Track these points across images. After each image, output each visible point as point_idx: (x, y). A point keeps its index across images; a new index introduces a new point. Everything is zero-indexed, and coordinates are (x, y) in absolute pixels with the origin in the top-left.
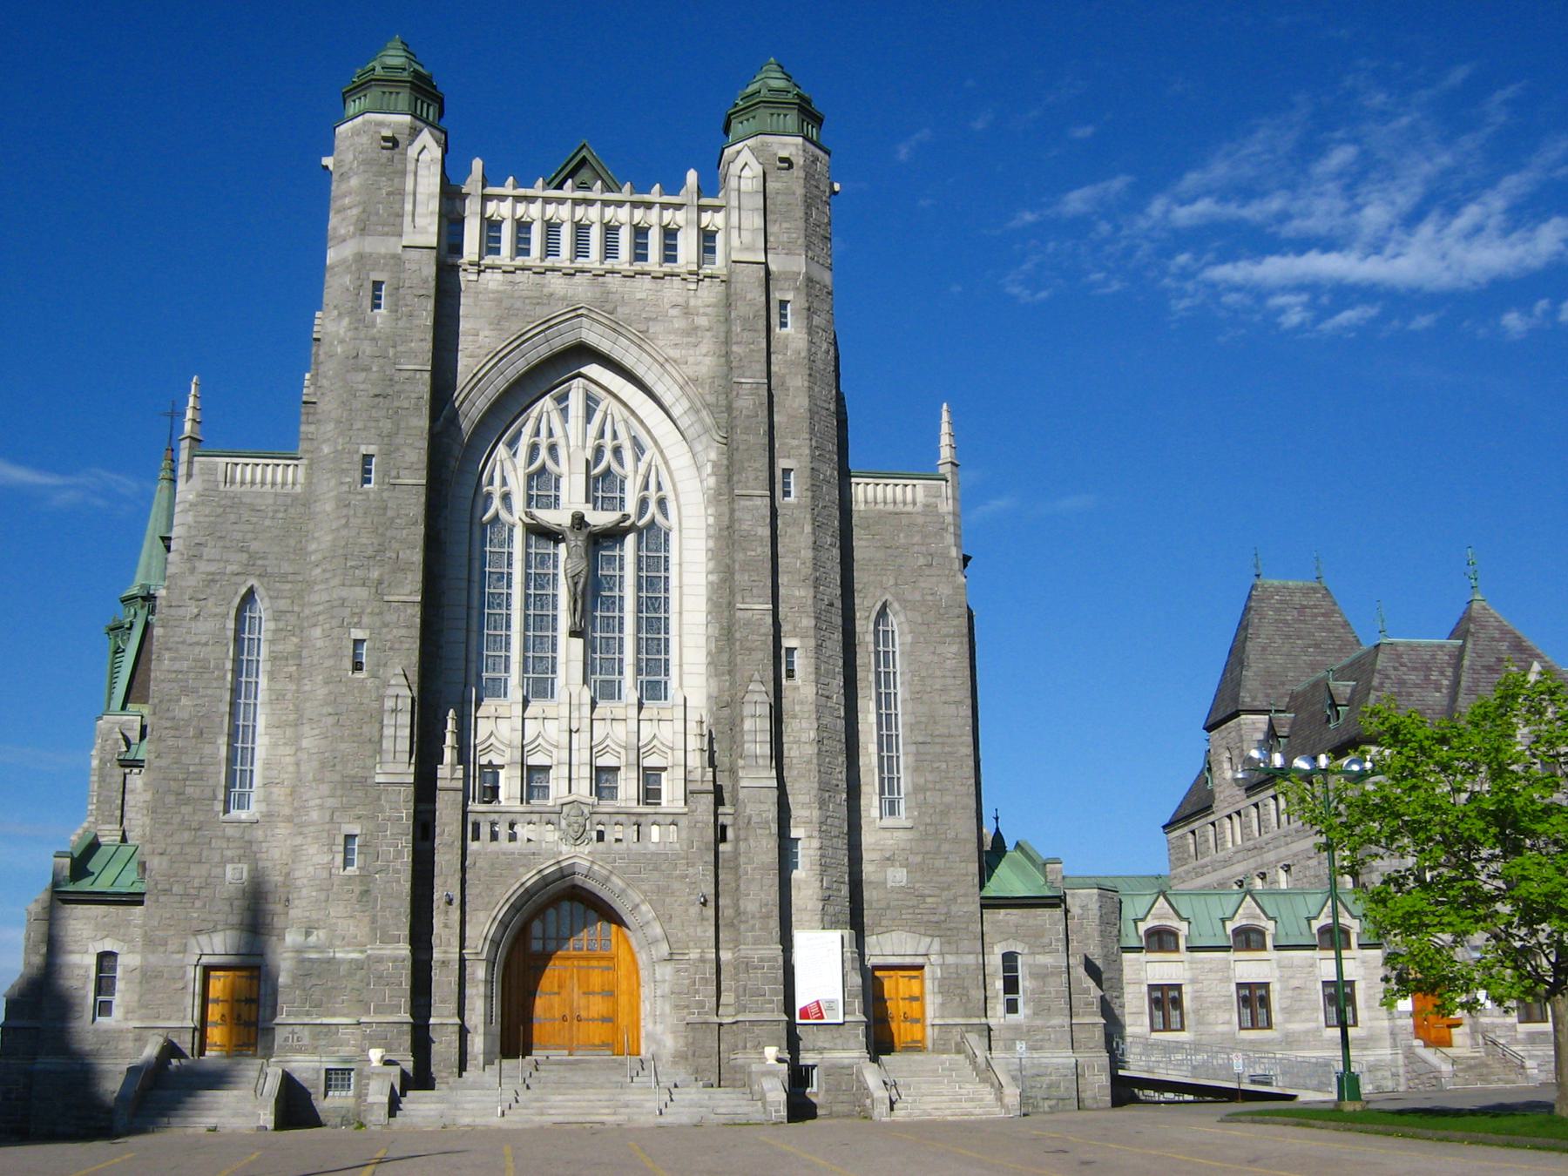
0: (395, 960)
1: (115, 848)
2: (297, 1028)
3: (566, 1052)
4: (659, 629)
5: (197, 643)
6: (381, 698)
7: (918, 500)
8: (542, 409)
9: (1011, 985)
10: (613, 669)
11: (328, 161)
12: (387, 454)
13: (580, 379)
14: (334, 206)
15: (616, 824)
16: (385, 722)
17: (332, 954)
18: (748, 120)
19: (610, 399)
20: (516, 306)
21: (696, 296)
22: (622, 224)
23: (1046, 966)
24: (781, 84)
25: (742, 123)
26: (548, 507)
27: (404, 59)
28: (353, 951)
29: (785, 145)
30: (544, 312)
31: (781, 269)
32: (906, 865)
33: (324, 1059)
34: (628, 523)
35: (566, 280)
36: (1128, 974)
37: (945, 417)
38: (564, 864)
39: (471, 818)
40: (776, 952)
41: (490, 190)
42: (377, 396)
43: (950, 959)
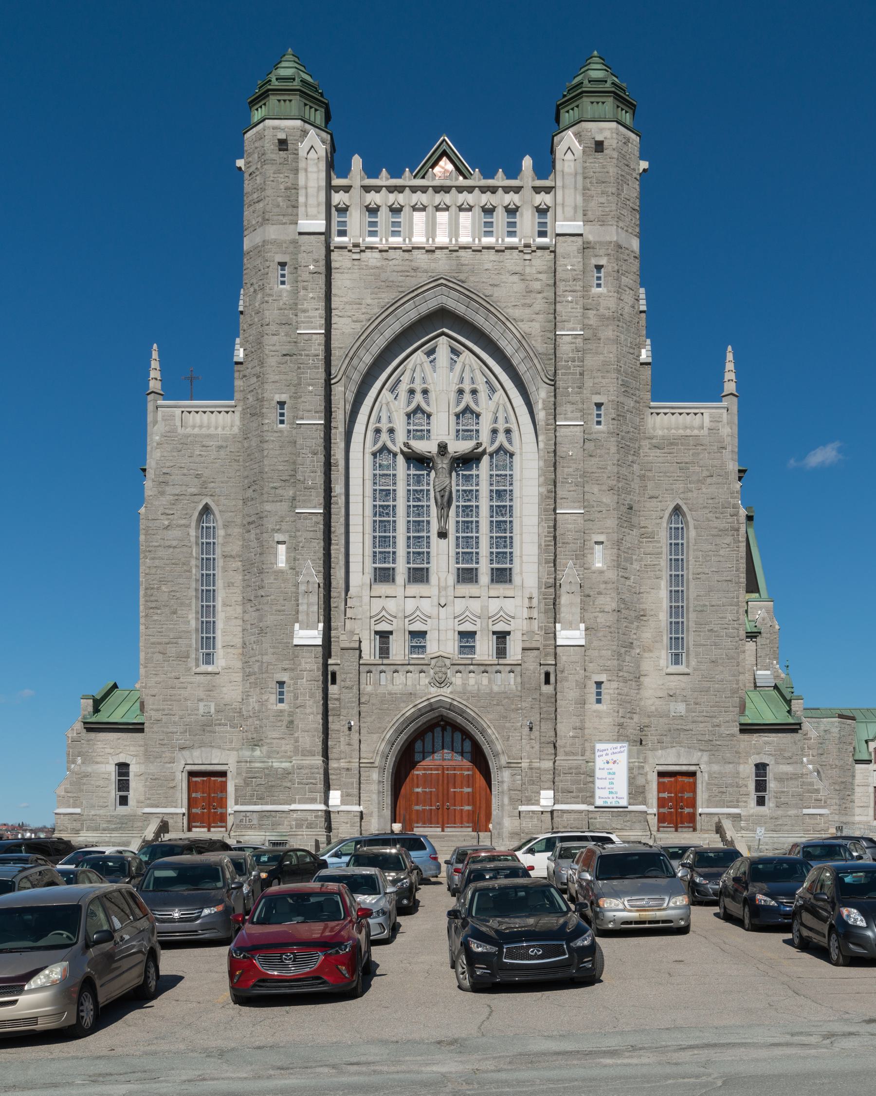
0: (311, 767)
1: (128, 692)
2: (248, 814)
3: (440, 829)
4: (505, 530)
5: (169, 547)
6: (297, 585)
7: (705, 425)
8: (415, 362)
9: (761, 786)
10: (472, 560)
11: (240, 163)
12: (296, 397)
13: (443, 337)
14: (247, 200)
15: (457, 672)
16: (300, 601)
17: (270, 764)
18: (573, 109)
19: (467, 352)
20: (391, 279)
21: (531, 266)
22: (403, 207)
23: (787, 774)
24: (599, 75)
25: (568, 112)
26: (421, 438)
27: (294, 70)
28: (286, 762)
29: (601, 130)
30: (412, 282)
31: (597, 239)
32: (685, 700)
33: (267, 834)
34: (480, 450)
35: (430, 256)
36: (859, 779)
37: (730, 356)
38: (432, 700)
39: (330, 668)
40: (317, 762)
41: (336, 182)
42: (285, 355)
43: (716, 768)
